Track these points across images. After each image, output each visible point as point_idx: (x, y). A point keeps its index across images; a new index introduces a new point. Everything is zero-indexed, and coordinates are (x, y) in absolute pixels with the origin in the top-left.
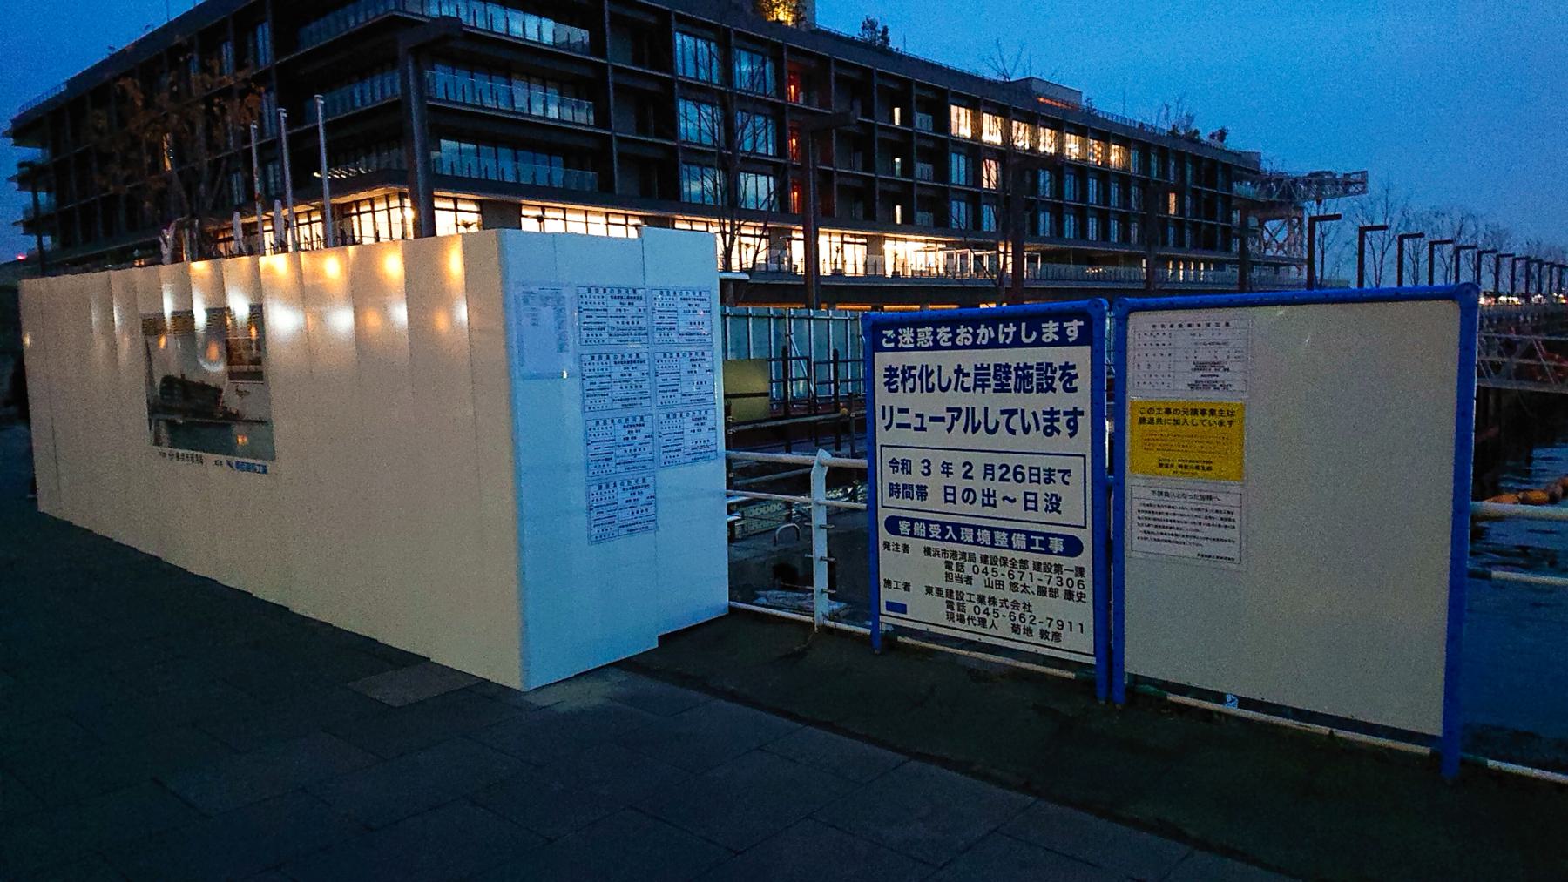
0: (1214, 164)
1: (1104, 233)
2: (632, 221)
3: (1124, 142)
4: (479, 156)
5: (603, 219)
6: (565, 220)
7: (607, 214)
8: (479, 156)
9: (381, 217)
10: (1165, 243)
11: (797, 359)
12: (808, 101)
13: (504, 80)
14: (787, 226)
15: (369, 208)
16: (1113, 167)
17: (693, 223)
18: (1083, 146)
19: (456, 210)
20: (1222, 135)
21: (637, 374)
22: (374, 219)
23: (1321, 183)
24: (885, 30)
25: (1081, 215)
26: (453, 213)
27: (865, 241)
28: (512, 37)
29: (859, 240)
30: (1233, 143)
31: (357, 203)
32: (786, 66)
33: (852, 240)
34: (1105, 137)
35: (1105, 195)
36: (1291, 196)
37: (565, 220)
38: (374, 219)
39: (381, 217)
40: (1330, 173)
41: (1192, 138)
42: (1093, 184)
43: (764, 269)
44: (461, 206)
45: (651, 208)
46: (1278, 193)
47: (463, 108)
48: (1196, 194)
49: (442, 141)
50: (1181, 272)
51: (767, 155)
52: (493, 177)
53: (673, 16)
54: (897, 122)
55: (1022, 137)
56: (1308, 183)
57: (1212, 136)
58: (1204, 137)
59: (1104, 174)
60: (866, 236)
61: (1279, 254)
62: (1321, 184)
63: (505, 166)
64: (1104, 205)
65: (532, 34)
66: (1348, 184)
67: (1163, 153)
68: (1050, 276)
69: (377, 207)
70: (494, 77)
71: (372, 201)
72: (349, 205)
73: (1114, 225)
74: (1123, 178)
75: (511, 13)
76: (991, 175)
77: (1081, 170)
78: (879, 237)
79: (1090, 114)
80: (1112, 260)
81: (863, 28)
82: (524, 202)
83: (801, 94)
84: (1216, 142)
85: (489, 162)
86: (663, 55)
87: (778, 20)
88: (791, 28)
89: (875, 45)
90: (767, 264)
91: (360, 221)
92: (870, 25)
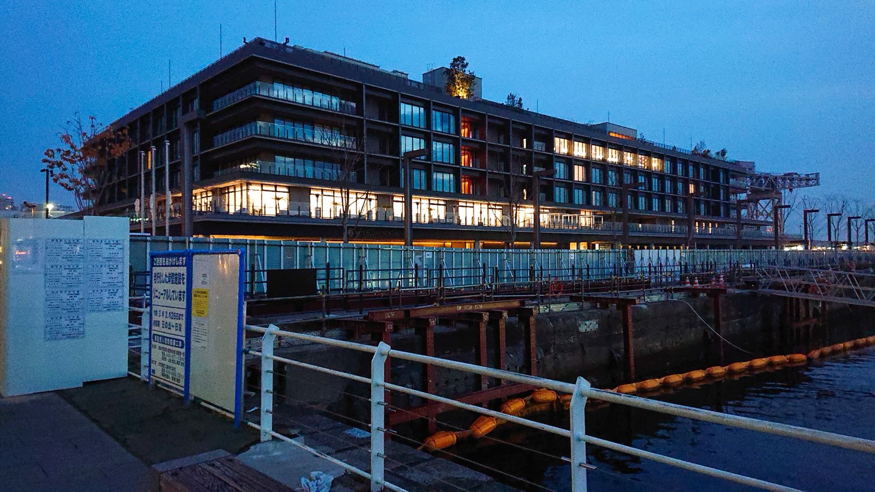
0: (717, 169)
1: (662, 207)
2: (440, 202)
3: (660, 157)
4: (295, 164)
5: (259, 188)
6: (333, 196)
7: (262, 185)
8: (295, 164)
9: (238, 194)
10: (699, 213)
11: (445, 269)
12: (474, 137)
13: (310, 127)
14: (391, 194)
15: (233, 190)
16: (654, 170)
17: (358, 194)
18: (635, 158)
19: (276, 191)
20: (723, 153)
21: (76, 274)
22: (235, 195)
23: (792, 180)
24: (520, 100)
25: (662, 199)
26: (274, 193)
27: (501, 207)
28: (316, 107)
29: (497, 207)
30: (730, 157)
31: (228, 188)
32: (461, 119)
33: (494, 207)
34: (649, 154)
35: (605, 178)
36: (773, 186)
37: (333, 196)
38: (235, 195)
39: (238, 194)
40: (796, 174)
41: (706, 155)
42: (655, 181)
43: (286, 214)
44: (278, 189)
45: (380, 190)
46: (766, 184)
47: (305, 144)
48: (706, 185)
49: (276, 157)
50: (710, 229)
51: (449, 163)
52: (292, 174)
53: (400, 95)
54: (525, 147)
55: (597, 153)
56: (784, 179)
57: (718, 153)
58: (713, 154)
59: (649, 174)
60: (502, 205)
61: (768, 219)
62: (792, 180)
63: (308, 169)
64: (727, 201)
65: (299, 100)
66: (811, 180)
67: (685, 163)
68: (663, 231)
69: (237, 190)
70: (286, 123)
71: (234, 187)
72: (225, 188)
73: (680, 204)
74: (661, 176)
75: (297, 91)
76: (579, 174)
77: (634, 171)
78: (389, 196)
79: (643, 142)
80: (652, 220)
81: (508, 99)
82: (460, 200)
83: (471, 132)
84: (720, 158)
85: (300, 168)
86: (395, 114)
87: (459, 97)
88: (465, 100)
89: (514, 108)
90: (288, 211)
91: (229, 196)
92: (511, 97)
